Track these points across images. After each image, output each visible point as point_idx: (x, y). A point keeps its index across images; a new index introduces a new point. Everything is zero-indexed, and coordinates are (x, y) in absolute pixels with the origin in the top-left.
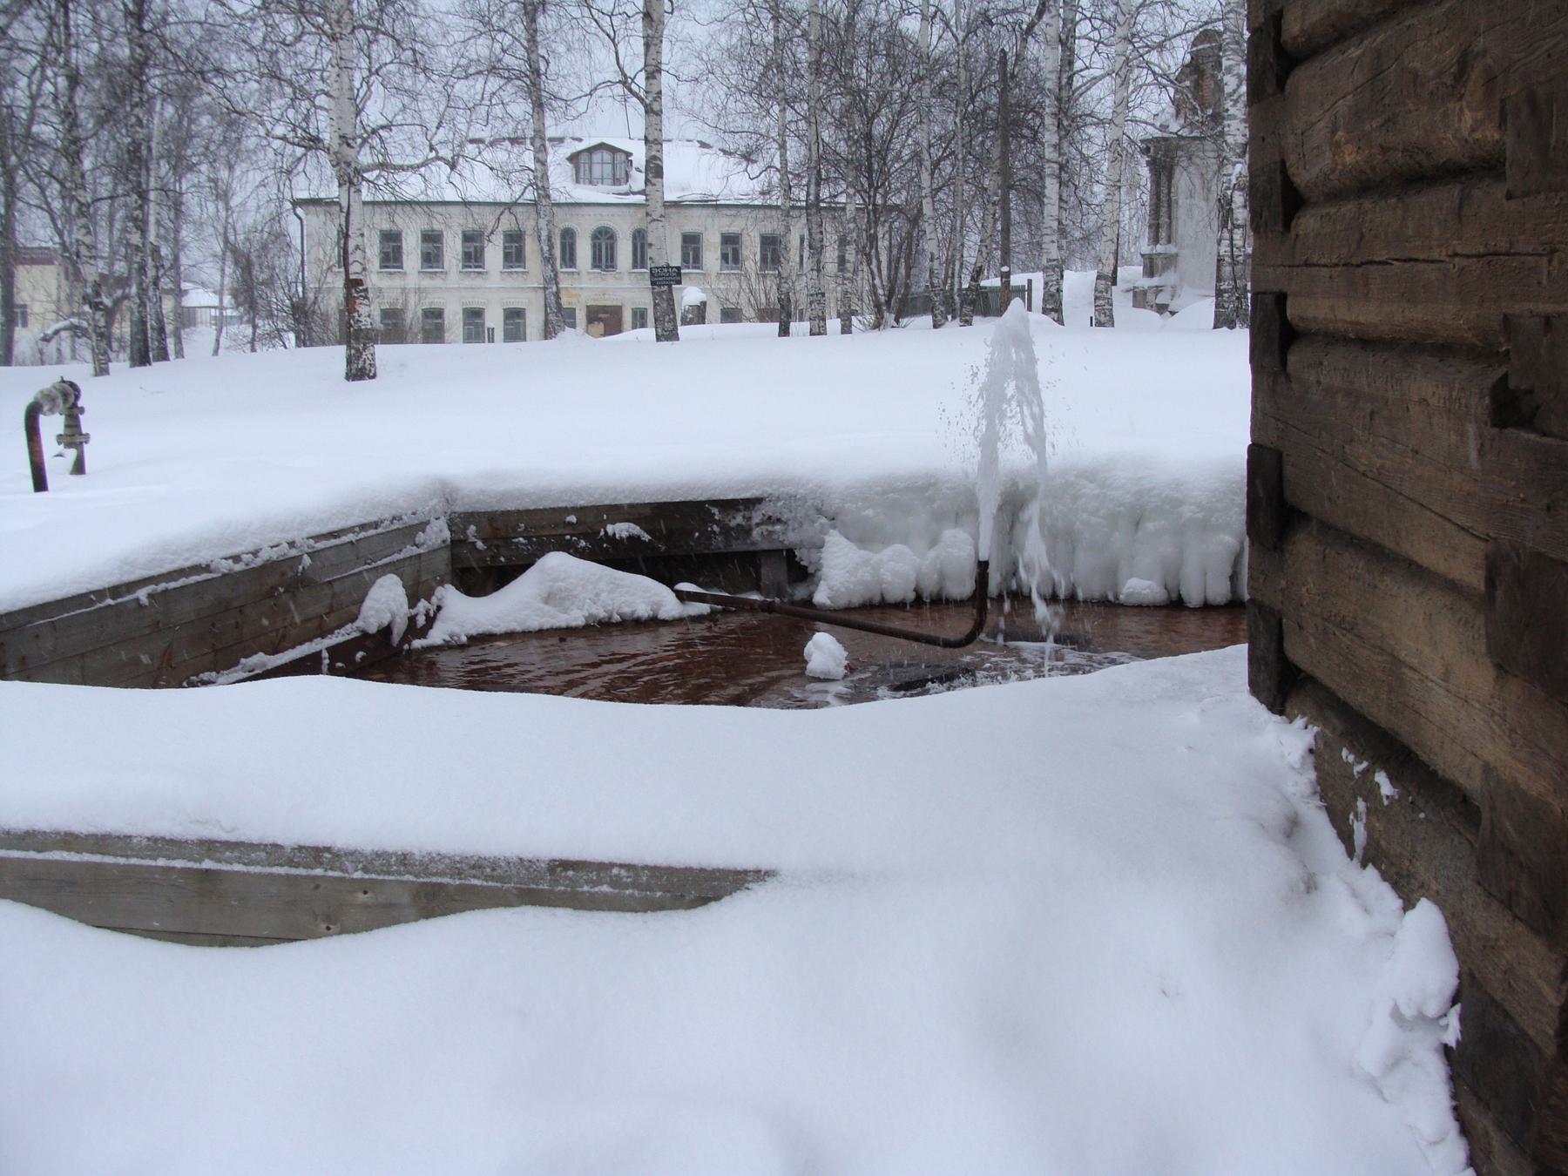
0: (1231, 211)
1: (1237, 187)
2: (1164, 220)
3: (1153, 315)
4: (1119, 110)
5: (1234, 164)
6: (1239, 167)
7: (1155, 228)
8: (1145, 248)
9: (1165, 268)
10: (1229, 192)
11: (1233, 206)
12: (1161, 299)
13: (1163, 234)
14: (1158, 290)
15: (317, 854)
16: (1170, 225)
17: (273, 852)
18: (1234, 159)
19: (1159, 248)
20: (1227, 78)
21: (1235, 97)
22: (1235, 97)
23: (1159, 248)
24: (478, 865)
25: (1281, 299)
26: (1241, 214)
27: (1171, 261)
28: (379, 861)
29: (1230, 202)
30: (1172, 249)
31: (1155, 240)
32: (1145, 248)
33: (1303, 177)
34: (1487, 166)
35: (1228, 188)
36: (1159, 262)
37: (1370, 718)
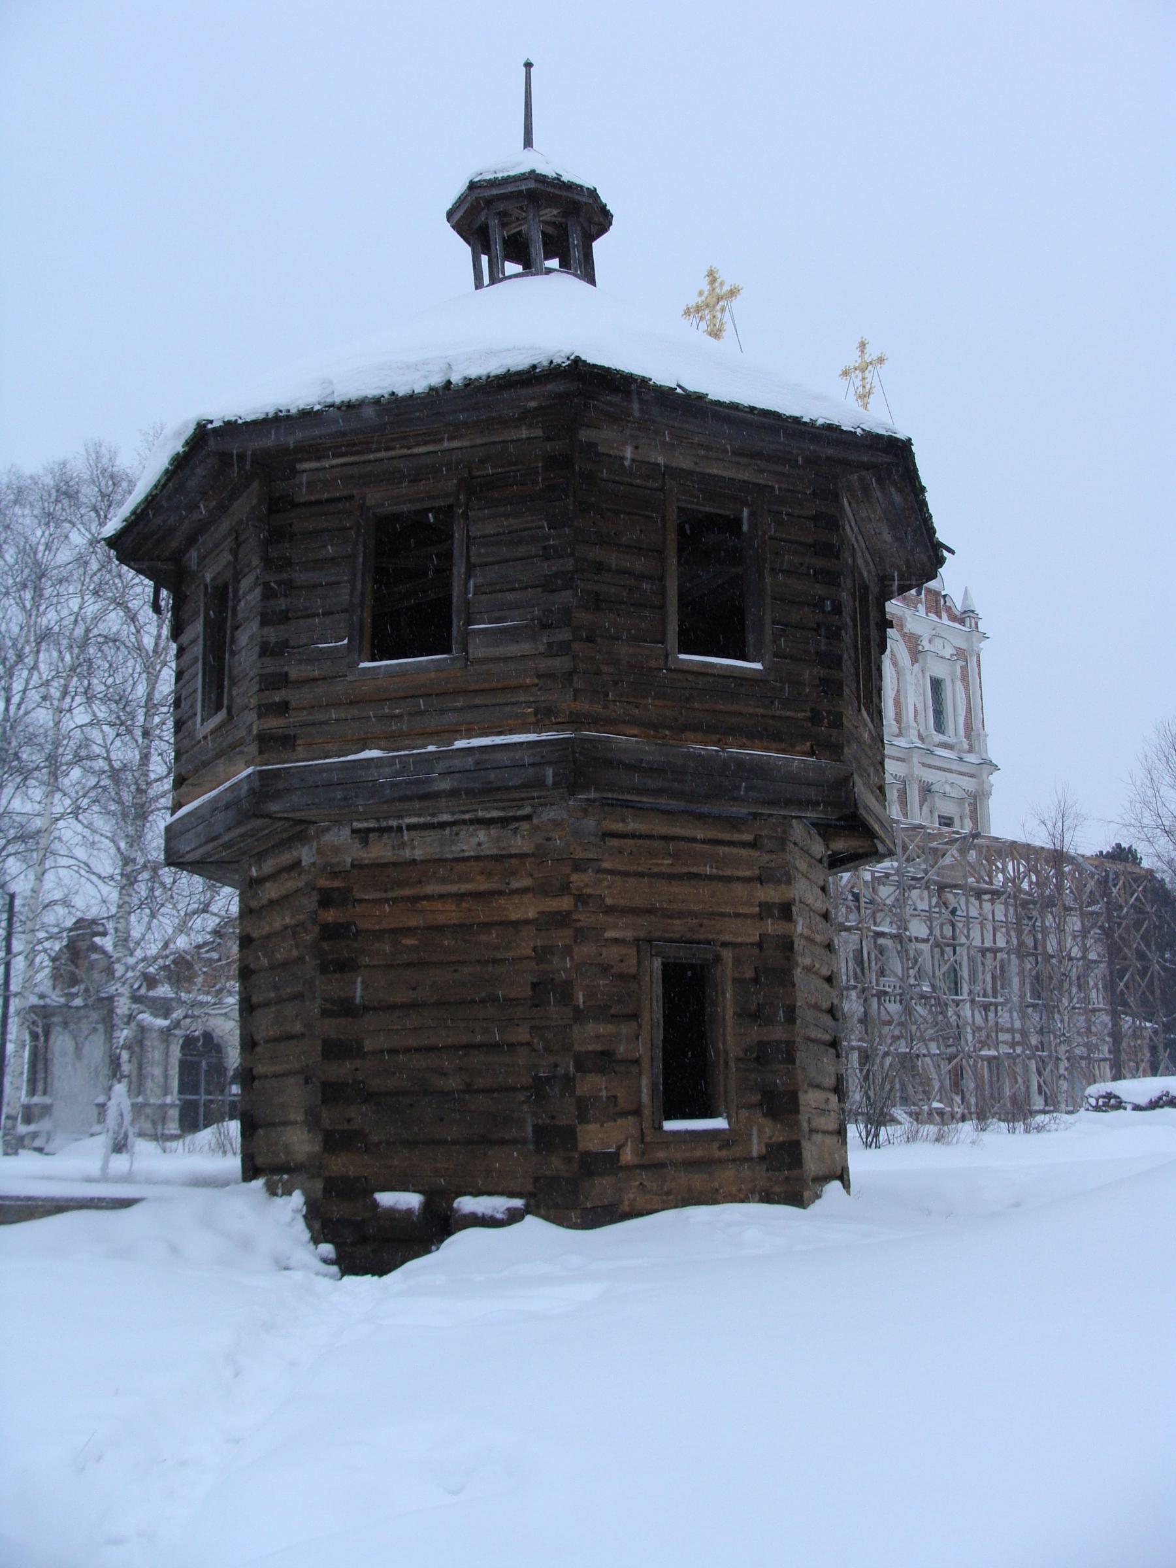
0: (119, 1065)
1: (124, 1047)
2: (41, 1075)
3: (37, 1155)
4: (26, 985)
5: (122, 1029)
6: (125, 1032)
7: (32, 1082)
8: (24, 1099)
9: (41, 1116)
10: (118, 1051)
11: (121, 1061)
12: (38, 1143)
13: (40, 1086)
14: (35, 1135)
15: (29, 1198)
16: (46, 1079)
17: (18, 1198)
18: (123, 1026)
19: (36, 1099)
20: (117, 966)
21: (123, 980)
22: (123, 980)
23: (36, 1099)
24: (72, 1199)
25: (251, 1069)
26: (677, 961)
27: (46, 1110)
28: (46, 1199)
29: (119, 1058)
30: (47, 1100)
31: (32, 1092)
32: (24, 1099)
33: (258, 1037)
34: (303, 1035)
35: (117, 1048)
36: (37, 1111)
37: (499, 175)
